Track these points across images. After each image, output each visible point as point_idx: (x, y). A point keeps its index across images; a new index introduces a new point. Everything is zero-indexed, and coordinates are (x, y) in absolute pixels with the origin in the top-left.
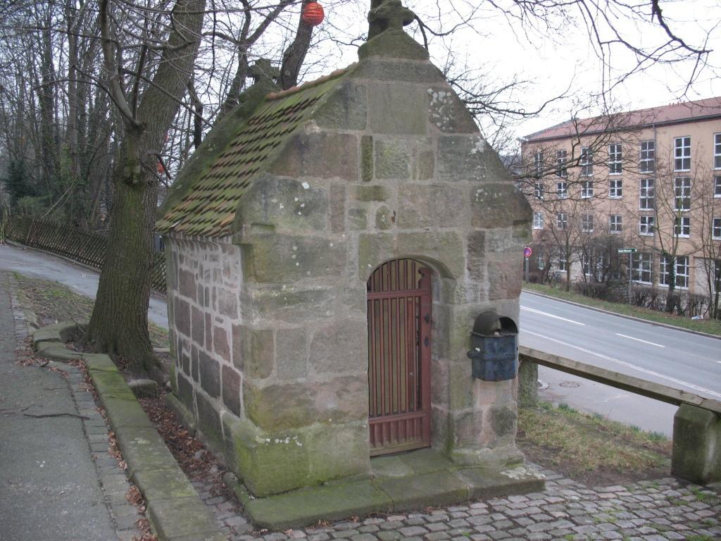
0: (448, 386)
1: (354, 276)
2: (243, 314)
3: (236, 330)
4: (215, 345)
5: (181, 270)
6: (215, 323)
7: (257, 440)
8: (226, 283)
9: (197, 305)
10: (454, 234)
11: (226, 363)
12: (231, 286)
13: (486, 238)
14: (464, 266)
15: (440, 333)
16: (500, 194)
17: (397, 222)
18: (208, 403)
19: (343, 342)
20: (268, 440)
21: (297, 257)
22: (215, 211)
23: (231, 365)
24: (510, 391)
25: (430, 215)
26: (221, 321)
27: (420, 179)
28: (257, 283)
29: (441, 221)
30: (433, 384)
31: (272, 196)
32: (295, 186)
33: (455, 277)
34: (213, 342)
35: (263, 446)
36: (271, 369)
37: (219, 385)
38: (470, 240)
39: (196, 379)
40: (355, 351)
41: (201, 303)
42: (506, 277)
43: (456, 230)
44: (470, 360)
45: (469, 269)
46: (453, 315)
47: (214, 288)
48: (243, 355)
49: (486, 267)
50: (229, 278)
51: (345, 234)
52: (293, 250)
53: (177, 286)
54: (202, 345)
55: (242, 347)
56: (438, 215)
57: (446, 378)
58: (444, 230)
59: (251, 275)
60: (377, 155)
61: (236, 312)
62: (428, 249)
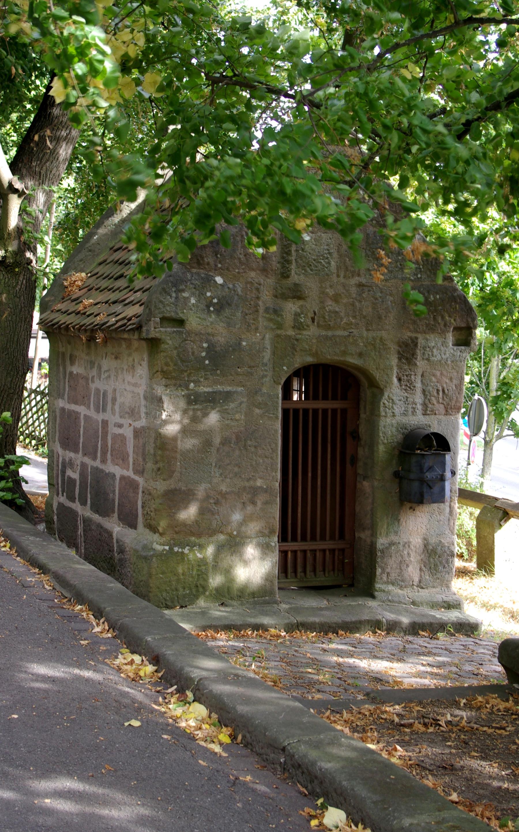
0: (372, 510)
1: (267, 379)
2: (147, 413)
3: (137, 433)
4: (112, 455)
5: (71, 373)
6: (113, 430)
7: (153, 547)
8: (128, 382)
9: (92, 413)
10: (381, 338)
11: (125, 473)
12: (135, 385)
13: (419, 345)
14: (393, 374)
15: (366, 450)
16: (438, 297)
17: (318, 323)
18: (100, 526)
19: (253, 449)
20: (167, 548)
21: (206, 355)
22: (109, 290)
23: (130, 473)
24: (447, 523)
25: (354, 317)
26: (120, 426)
27: (344, 277)
28: (164, 379)
29: (368, 323)
30: (357, 509)
31: (183, 291)
32: (208, 281)
33: (382, 387)
34: (109, 452)
35: (160, 555)
36: (173, 472)
37: (114, 500)
38: (400, 346)
39: (83, 503)
40: (266, 459)
41: (97, 410)
42: (443, 391)
43: (384, 334)
44: (397, 480)
45: (399, 380)
46: (378, 429)
47: (115, 390)
48: (144, 460)
49: (420, 377)
50: (133, 376)
51: (260, 333)
52: (203, 347)
53: (64, 395)
54: (95, 459)
55: (144, 450)
56: (365, 317)
57: (370, 500)
58: (371, 334)
59: (157, 371)
60: (297, 251)
61: (139, 413)
62: (352, 354)
